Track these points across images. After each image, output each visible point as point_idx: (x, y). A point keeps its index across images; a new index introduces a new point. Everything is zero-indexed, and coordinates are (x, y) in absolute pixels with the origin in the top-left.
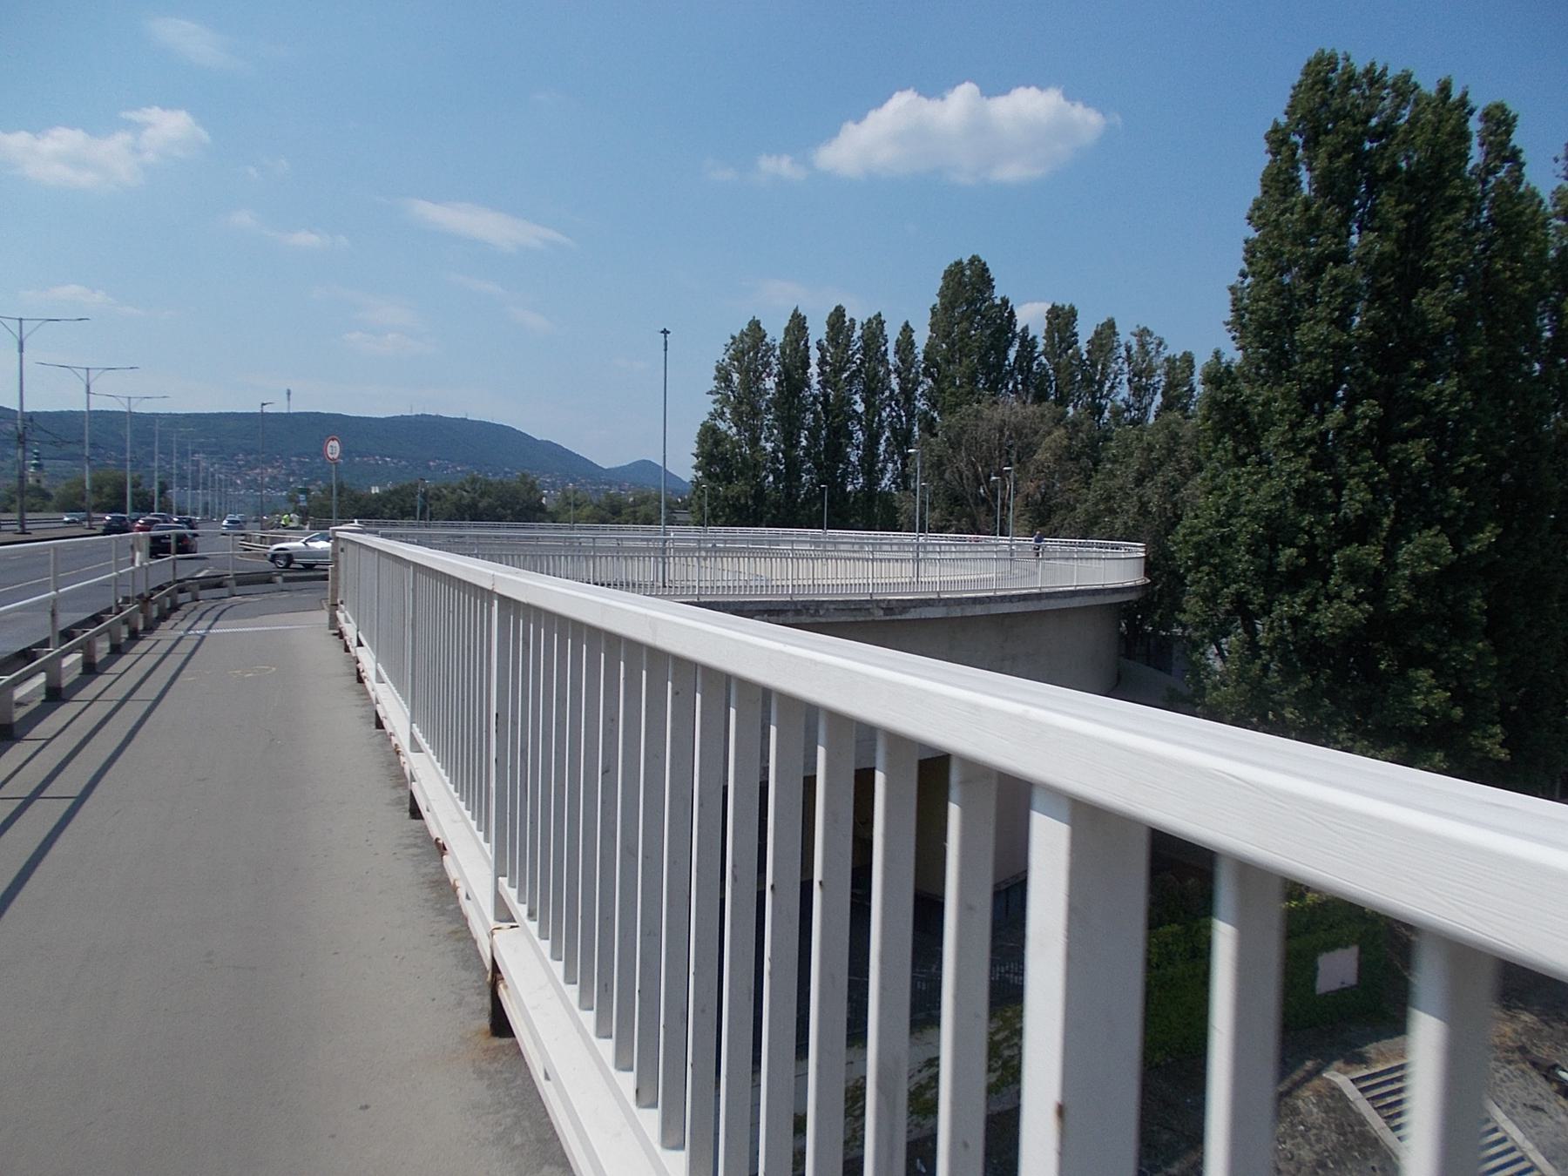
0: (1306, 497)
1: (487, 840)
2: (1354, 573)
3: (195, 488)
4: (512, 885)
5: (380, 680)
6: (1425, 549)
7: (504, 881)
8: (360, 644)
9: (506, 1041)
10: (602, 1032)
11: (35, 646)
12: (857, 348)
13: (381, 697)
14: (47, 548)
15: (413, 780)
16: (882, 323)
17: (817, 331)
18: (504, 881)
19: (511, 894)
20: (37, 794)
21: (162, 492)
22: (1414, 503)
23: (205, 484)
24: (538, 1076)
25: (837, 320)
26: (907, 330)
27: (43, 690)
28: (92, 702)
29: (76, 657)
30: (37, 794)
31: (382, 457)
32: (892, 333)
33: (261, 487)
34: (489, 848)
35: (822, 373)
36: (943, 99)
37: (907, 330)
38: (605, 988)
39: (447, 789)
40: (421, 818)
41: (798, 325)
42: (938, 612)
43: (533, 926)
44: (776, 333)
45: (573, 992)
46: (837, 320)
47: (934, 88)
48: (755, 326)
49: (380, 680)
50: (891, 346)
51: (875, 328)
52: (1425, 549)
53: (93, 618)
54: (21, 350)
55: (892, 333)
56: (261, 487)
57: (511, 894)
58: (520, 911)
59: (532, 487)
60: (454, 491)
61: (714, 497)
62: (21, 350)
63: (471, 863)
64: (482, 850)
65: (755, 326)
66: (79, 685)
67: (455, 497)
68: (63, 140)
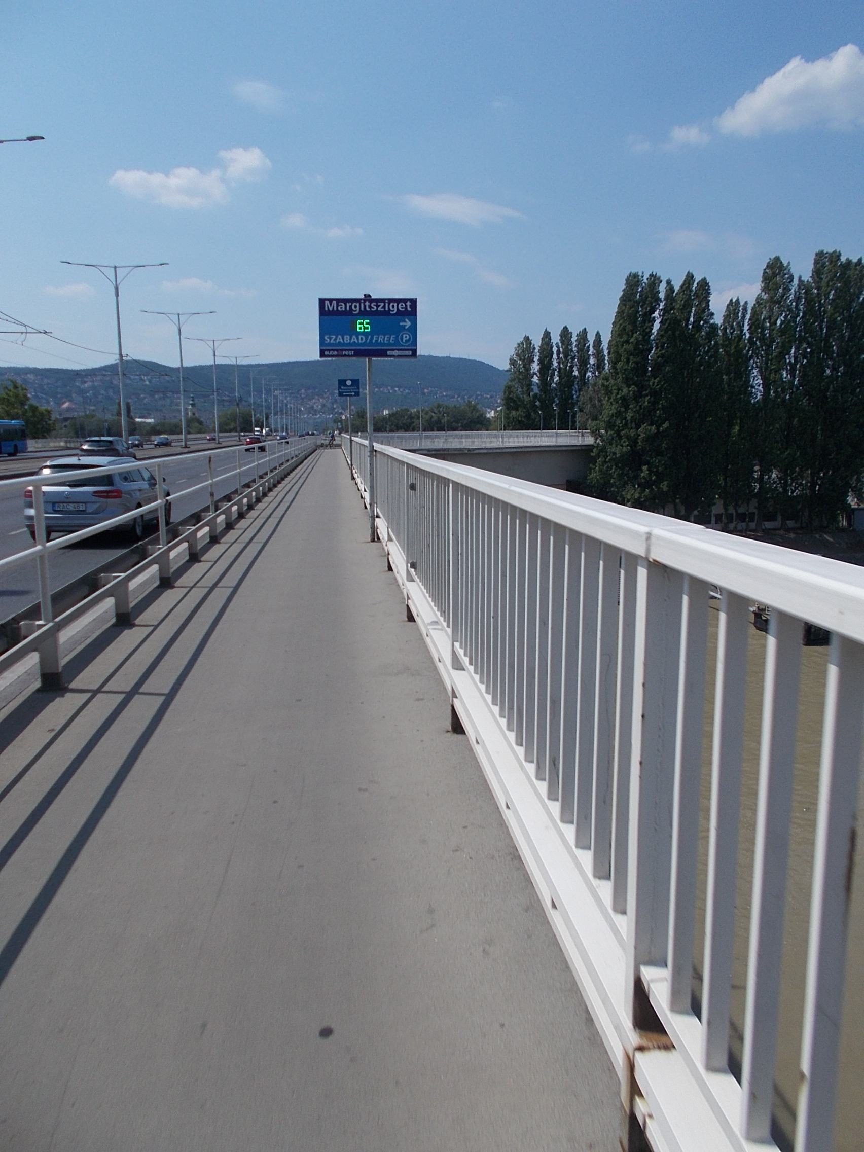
0: (618, 414)
1: (448, 626)
2: (628, 437)
3: (276, 414)
4: (461, 648)
5: (457, 665)
6: (645, 430)
7: (649, 973)
8: (390, 539)
9: (460, 737)
10: (552, 796)
11: (16, 620)
12: (574, 347)
13: (413, 595)
14: (234, 452)
15: (408, 598)
16: (586, 333)
17: (556, 339)
18: (457, 645)
19: (461, 652)
20: (215, 585)
21: (267, 418)
22: (645, 416)
23: (282, 411)
24: (401, 584)
25: (565, 334)
26: (598, 335)
27: (208, 536)
28: (192, 588)
29: (223, 517)
30: (215, 585)
31: (393, 388)
32: (591, 338)
33: (316, 412)
34: (626, 924)
35: (558, 357)
36: (831, 59)
37: (598, 335)
38: (554, 762)
39: (436, 615)
40: (414, 621)
41: (547, 335)
42: (485, 451)
43: (471, 668)
44: (537, 342)
45: (531, 768)
46: (565, 334)
47: (818, 51)
48: (527, 339)
49: (457, 665)
50: (591, 343)
51: (583, 335)
52: (645, 430)
53: (193, 516)
54: (117, 295)
55: (591, 338)
56: (316, 412)
57: (461, 652)
58: (466, 660)
59: (474, 409)
60: (427, 413)
61: (507, 418)
62: (117, 295)
63: (440, 641)
64: (446, 632)
65: (527, 339)
66: (206, 548)
67: (427, 417)
68: (184, 176)
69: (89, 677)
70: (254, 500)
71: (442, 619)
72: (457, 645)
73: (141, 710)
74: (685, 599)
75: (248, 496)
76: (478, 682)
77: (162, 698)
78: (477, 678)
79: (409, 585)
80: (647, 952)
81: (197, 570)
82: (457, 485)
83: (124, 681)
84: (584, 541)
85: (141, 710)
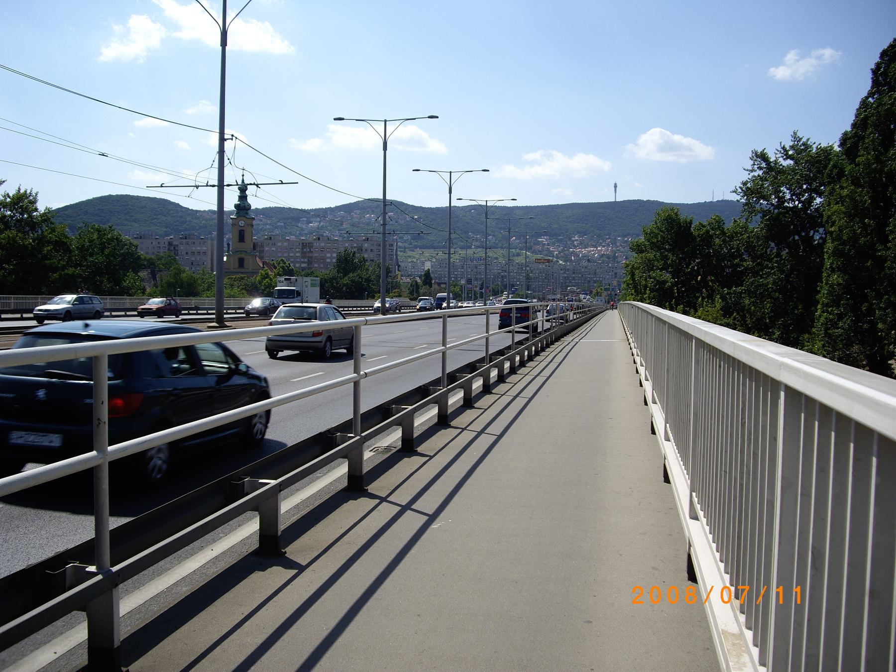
5: (694, 517)
13: (655, 415)
58: (701, 514)
69: (458, 422)
70: (526, 358)
71: (749, 635)
72: (694, 494)
73: (411, 522)
74: (874, 460)
75: (521, 354)
76: (711, 541)
77: (426, 518)
78: (707, 528)
79: (666, 443)
80: (666, 422)
81: (469, 415)
82: (794, 395)
83: (402, 496)
84: (782, 394)
85: (411, 522)
